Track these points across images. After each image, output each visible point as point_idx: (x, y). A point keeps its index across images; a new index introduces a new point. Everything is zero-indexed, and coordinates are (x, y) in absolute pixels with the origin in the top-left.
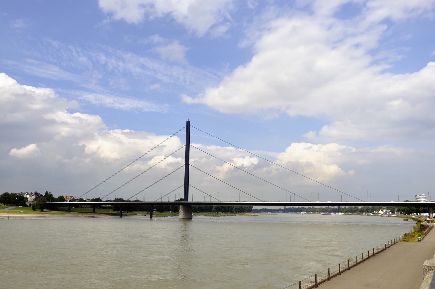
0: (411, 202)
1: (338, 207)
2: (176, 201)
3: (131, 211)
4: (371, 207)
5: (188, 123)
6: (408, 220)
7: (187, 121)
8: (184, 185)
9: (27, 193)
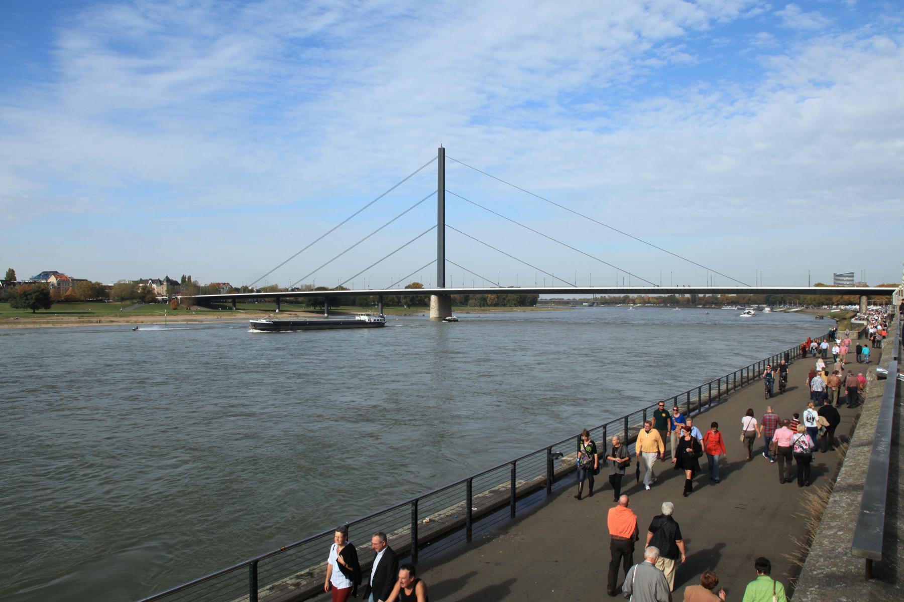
0: (827, 286)
1: (692, 296)
3: (336, 307)
5: (442, 152)
6: (824, 318)
7: (439, 148)
9: (150, 279)
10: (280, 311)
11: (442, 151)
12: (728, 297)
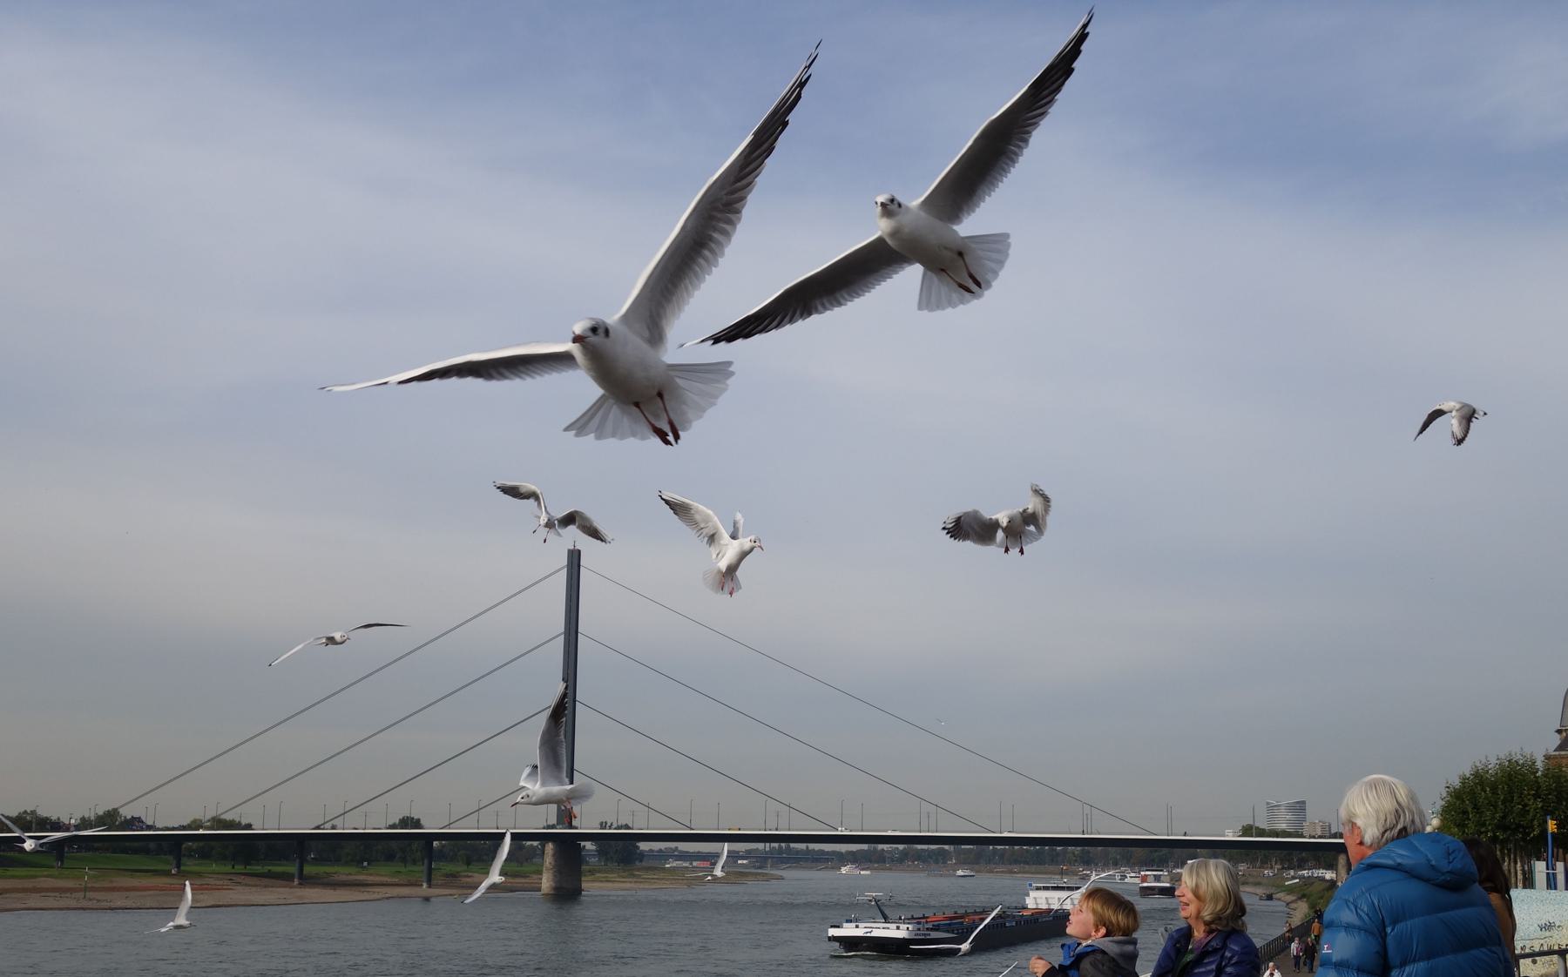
2: (549, 827)
7: (569, 550)
8: (563, 636)
12: (917, 849)
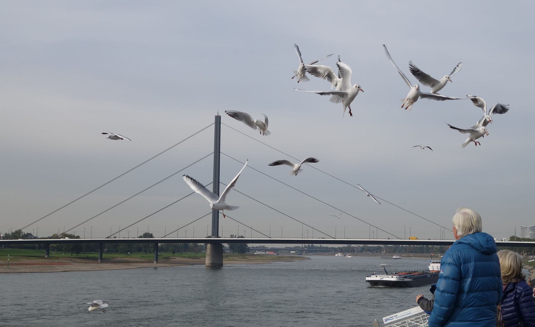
4: (413, 246)
7: (216, 116)
10: (48, 257)
11: (218, 118)
